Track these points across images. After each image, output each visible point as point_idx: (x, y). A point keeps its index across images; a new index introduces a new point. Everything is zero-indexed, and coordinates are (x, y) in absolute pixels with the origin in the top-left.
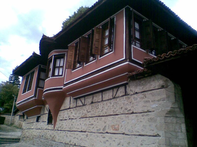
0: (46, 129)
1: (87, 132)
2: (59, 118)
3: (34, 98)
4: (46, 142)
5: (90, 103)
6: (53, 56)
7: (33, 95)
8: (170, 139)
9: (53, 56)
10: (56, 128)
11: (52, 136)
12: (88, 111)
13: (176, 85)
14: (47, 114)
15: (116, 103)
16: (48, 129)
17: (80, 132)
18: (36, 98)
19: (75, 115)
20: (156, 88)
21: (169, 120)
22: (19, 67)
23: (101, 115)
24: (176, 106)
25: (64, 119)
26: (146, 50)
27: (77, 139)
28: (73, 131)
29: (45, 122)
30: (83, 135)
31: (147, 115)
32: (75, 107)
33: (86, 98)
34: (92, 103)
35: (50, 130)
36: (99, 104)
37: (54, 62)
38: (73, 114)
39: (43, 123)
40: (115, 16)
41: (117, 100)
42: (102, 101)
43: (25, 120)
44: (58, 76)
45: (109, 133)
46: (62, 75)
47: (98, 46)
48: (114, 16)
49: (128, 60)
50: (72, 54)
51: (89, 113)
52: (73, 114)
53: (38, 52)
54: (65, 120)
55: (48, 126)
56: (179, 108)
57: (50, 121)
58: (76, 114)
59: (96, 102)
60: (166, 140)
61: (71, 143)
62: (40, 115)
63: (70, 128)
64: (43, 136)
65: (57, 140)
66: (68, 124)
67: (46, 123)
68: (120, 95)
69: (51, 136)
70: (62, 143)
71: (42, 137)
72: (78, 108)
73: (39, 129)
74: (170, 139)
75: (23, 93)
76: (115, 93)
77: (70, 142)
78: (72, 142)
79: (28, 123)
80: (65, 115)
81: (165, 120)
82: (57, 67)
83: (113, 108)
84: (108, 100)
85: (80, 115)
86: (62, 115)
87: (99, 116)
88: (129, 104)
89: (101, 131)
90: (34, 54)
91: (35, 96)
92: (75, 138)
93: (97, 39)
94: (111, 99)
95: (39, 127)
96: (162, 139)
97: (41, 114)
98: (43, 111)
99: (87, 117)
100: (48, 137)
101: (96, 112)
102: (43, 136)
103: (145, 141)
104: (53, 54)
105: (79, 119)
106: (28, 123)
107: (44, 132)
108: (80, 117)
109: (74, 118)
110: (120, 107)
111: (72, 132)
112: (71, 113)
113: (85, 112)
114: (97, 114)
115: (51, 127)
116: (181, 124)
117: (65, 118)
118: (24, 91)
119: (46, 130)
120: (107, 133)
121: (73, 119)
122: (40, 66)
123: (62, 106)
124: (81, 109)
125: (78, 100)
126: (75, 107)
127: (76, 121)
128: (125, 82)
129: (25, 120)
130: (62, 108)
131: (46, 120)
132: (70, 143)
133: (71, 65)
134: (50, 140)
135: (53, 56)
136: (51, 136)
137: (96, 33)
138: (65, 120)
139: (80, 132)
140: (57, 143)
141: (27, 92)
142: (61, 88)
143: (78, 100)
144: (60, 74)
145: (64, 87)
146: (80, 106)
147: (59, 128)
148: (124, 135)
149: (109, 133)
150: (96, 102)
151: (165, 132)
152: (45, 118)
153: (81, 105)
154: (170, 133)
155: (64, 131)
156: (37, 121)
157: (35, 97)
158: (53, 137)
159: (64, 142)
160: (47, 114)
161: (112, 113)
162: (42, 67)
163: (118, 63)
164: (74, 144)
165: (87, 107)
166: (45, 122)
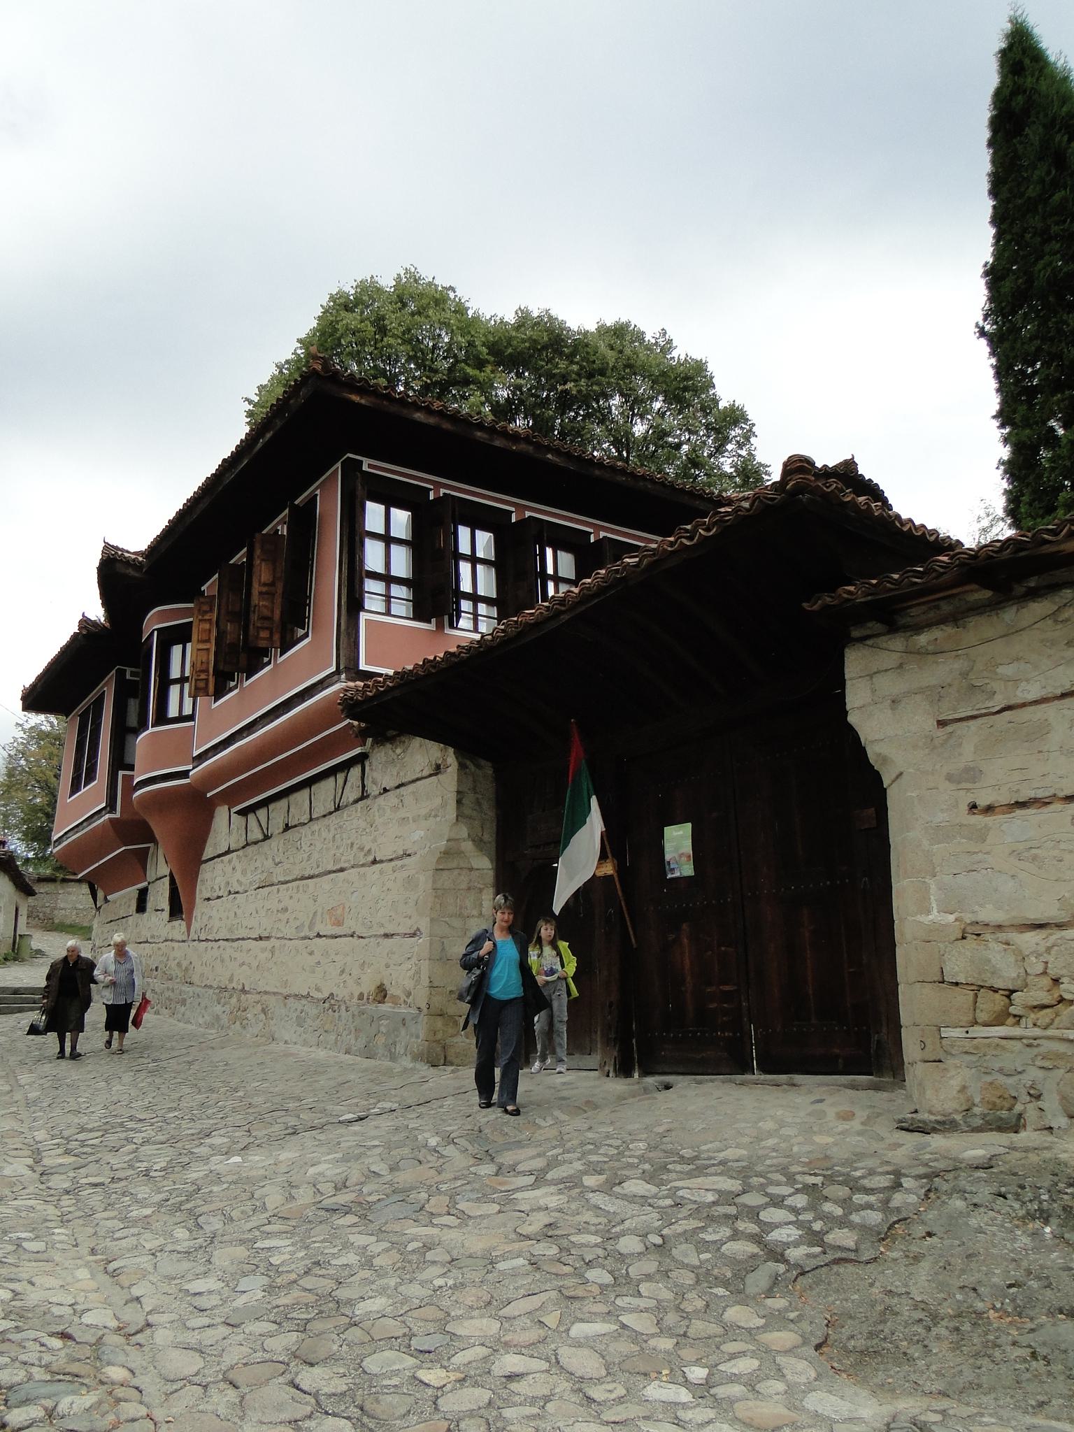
0: (166, 941)
1: (272, 939)
2: (202, 891)
3: (107, 816)
4: (168, 989)
5: (281, 830)
6: (156, 633)
7: (104, 805)
8: (445, 941)
9: (153, 632)
10: (193, 936)
11: (185, 964)
12: (277, 860)
13: (468, 763)
14: (166, 876)
15: (341, 827)
16: (172, 940)
17: (255, 939)
18: (118, 815)
19: (243, 879)
20: (426, 773)
21: (446, 880)
22: (34, 686)
23: (307, 876)
24: (463, 831)
25: (215, 895)
26: (433, 620)
27: (249, 965)
28: (239, 939)
29: (163, 910)
30: (264, 950)
31: (402, 867)
32: (243, 847)
33: (271, 807)
34: (287, 828)
35: (179, 941)
36: (303, 830)
37: (159, 660)
38: (238, 875)
39: (157, 920)
40: (318, 492)
41: (343, 817)
42: (311, 819)
43: (100, 907)
44: (181, 719)
45: (324, 936)
46: (191, 718)
47: (272, 612)
48: (102, 687)
49: (343, 676)
50: (210, 630)
51: (279, 870)
52: (238, 875)
53: (97, 612)
54: (219, 897)
55: (173, 927)
56: (473, 840)
57: (177, 909)
58: (244, 872)
59: (295, 826)
60: (431, 944)
61: (234, 985)
62: (144, 884)
63: (231, 930)
64: (157, 969)
65: (195, 979)
66: (226, 913)
67: (166, 915)
68: (351, 800)
69: (179, 965)
70: (211, 987)
71: (155, 973)
72: (250, 849)
73: (147, 942)
74: (445, 941)
75: (73, 792)
76: (341, 791)
77: (231, 980)
78: (235, 980)
79: (111, 921)
80: (218, 880)
81: (434, 882)
82: (176, 681)
83: (333, 846)
84: (324, 816)
85: (259, 878)
86: (213, 877)
87: (303, 878)
88: (367, 830)
89: (305, 932)
90: (85, 623)
91: (111, 806)
92: (243, 964)
93: (265, 585)
94: (331, 813)
95: (146, 934)
96: (423, 941)
97: (149, 879)
98: (153, 867)
99: (272, 885)
100: (173, 972)
101: (295, 864)
102: (157, 969)
103: (394, 953)
104: (154, 622)
105: (253, 892)
106: (111, 921)
107: (161, 953)
108: (257, 886)
109: (241, 890)
110: (349, 842)
111: (235, 944)
112: (234, 869)
113: (269, 863)
114: (297, 873)
115: (180, 925)
116: (481, 890)
117: (218, 890)
118: (75, 788)
119: (165, 943)
120: (319, 936)
121: (237, 893)
122: (121, 674)
123: (208, 844)
124: (259, 853)
125: (249, 816)
126: (243, 847)
127: (247, 901)
128: (358, 751)
129: (100, 907)
130: (209, 852)
131: (167, 908)
132: (230, 987)
133: (207, 680)
134: (178, 980)
135: (156, 633)
136: (179, 965)
137: (263, 560)
138: (219, 897)
139: (255, 939)
140: (198, 990)
141: (83, 791)
142: (185, 774)
143: (251, 817)
144: (187, 711)
145: (193, 768)
146: (256, 843)
147: (203, 931)
148: (355, 940)
149: (324, 936)
150: (295, 826)
151: (432, 920)
152: (160, 897)
153: (260, 837)
154: (445, 922)
155: (216, 941)
156: (141, 907)
157: (110, 812)
158: (187, 969)
159: (215, 985)
160: (166, 876)
161: (330, 867)
162: (128, 677)
163: (221, 747)
164: (240, 987)
165: (273, 843)
166: (163, 910)
